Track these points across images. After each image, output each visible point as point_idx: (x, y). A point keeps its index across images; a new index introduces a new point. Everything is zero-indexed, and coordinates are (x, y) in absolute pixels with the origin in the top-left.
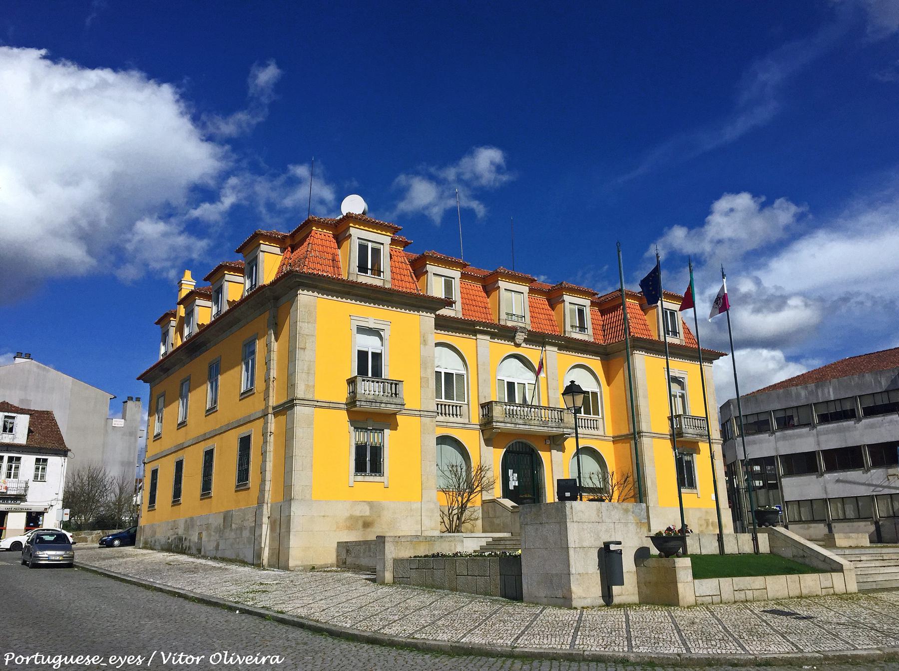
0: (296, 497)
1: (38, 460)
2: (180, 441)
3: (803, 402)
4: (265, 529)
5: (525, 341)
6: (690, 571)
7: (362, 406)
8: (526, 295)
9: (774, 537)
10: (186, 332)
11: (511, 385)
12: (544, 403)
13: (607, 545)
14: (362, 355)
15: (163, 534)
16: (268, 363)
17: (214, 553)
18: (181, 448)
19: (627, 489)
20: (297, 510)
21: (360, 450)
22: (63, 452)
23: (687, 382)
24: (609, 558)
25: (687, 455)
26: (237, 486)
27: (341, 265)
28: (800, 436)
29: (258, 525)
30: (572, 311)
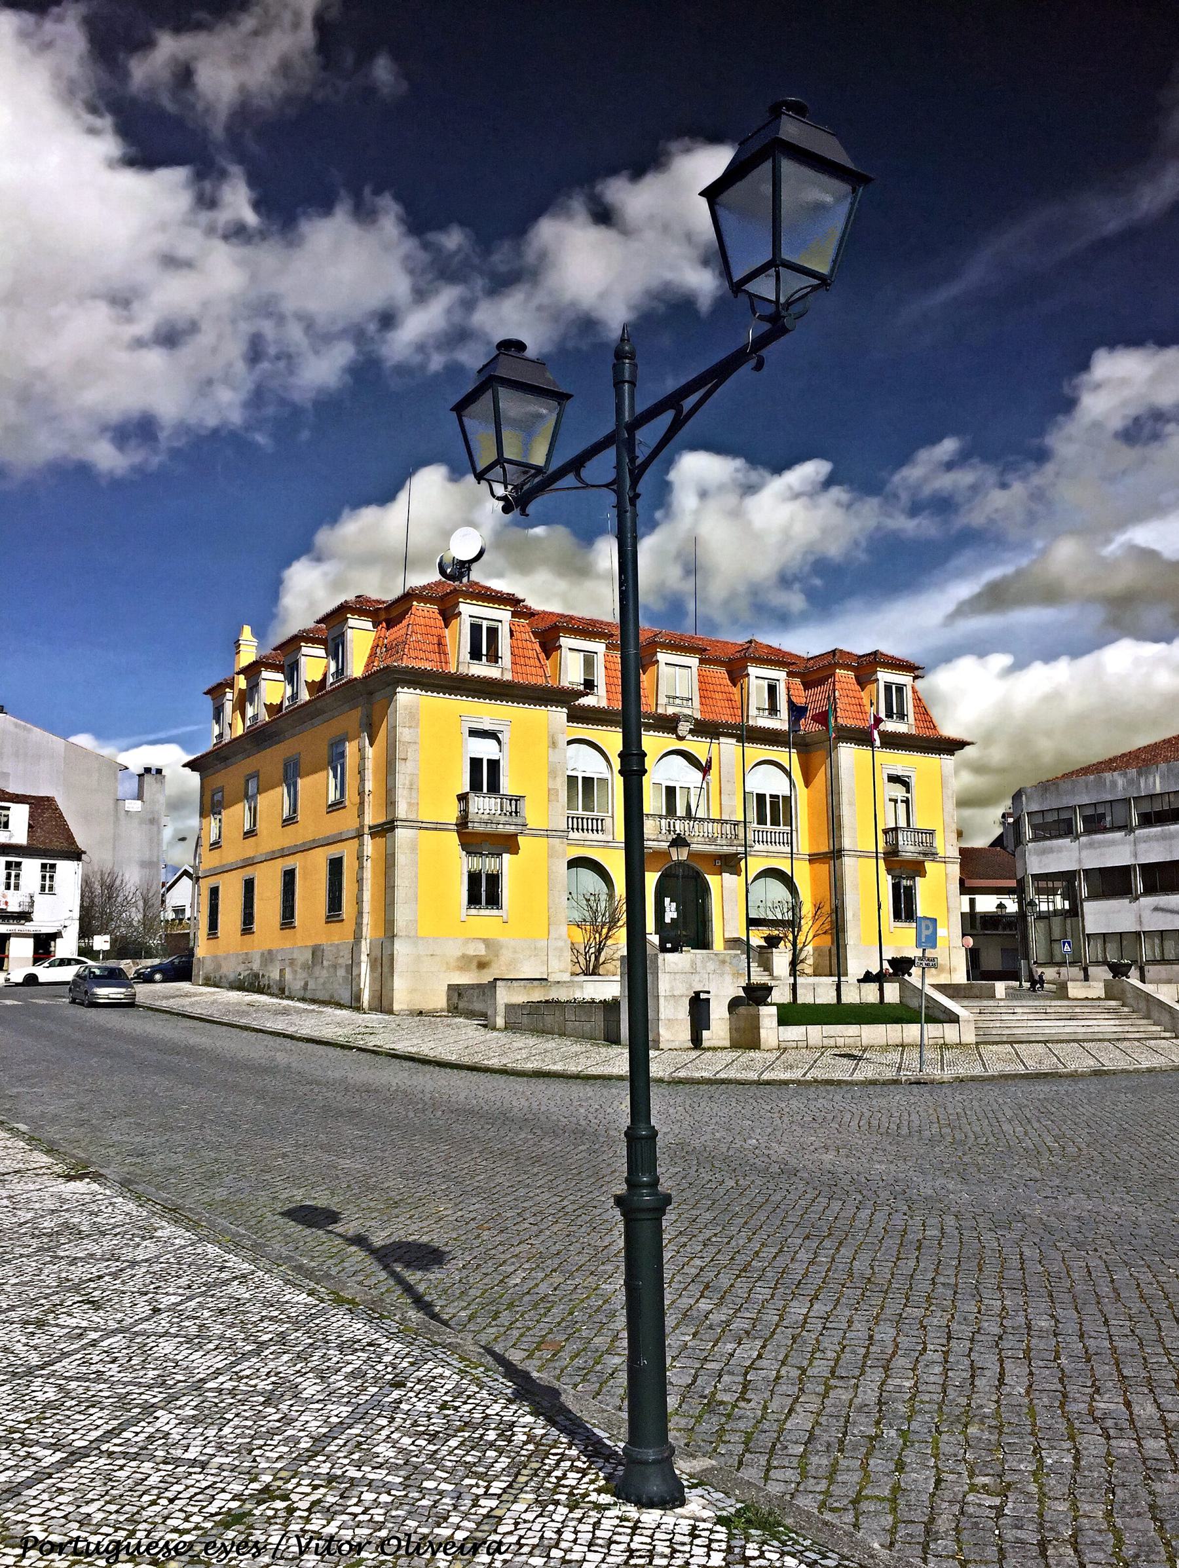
0: (400, 934)
1: (44, 866)
2: (249, 853)
3: (1120, 795)
4: (365, 968)
5: (691, 731)
6: (776, 1019)
7: (475, 827)
8: (695, 670)
9: (905, 987)
10: (250, 711)
11: (671, 792)
12: (715, 815)
13: (697, 994)
14: (476, 763)
15: (232, 969)
16: (361, 772)
17: (301, 994)
18: (249, 863)
19: (819, 922)
20: (401, 949)
21: (474, 879)
22: (76, 854)
23: (913, 783)
24: (699, 1007)
25: (907, 878)
26: (328, 917)
27: (449, 649)
28: (1113, 843)
29: (354, 963)
30: (759, 688)
